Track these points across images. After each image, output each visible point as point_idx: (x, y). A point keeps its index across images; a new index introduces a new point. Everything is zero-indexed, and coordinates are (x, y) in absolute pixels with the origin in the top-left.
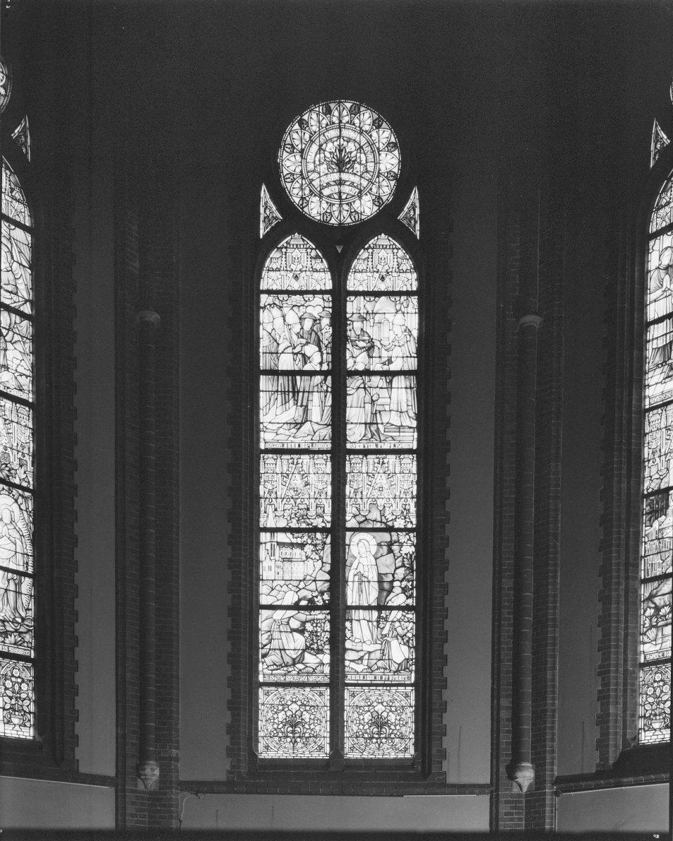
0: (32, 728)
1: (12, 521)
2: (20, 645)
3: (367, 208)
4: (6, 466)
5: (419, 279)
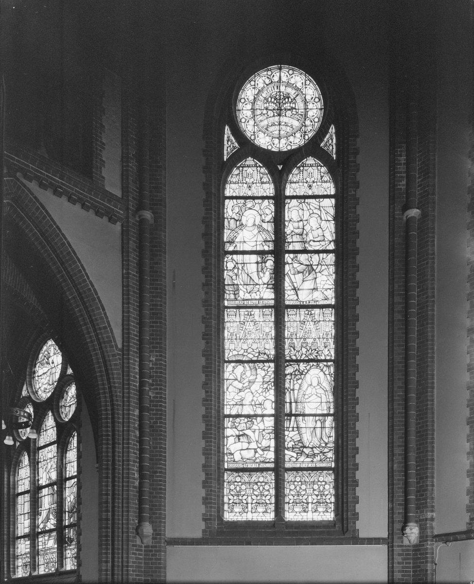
0: (332, 513)
1: (319, 383)
2: (324, 461)
3: (297, 141)
4: (315, 350)
5: (336, 187)
